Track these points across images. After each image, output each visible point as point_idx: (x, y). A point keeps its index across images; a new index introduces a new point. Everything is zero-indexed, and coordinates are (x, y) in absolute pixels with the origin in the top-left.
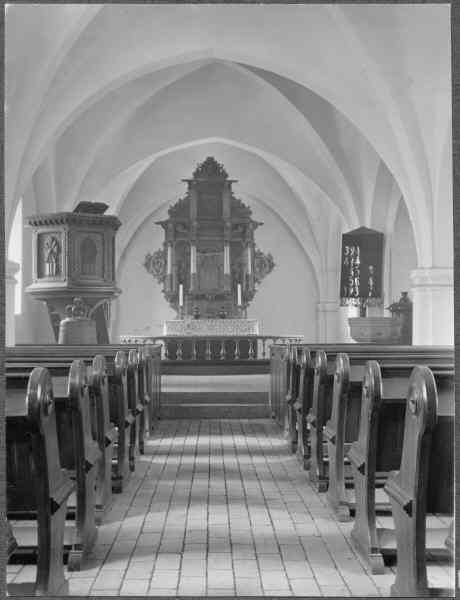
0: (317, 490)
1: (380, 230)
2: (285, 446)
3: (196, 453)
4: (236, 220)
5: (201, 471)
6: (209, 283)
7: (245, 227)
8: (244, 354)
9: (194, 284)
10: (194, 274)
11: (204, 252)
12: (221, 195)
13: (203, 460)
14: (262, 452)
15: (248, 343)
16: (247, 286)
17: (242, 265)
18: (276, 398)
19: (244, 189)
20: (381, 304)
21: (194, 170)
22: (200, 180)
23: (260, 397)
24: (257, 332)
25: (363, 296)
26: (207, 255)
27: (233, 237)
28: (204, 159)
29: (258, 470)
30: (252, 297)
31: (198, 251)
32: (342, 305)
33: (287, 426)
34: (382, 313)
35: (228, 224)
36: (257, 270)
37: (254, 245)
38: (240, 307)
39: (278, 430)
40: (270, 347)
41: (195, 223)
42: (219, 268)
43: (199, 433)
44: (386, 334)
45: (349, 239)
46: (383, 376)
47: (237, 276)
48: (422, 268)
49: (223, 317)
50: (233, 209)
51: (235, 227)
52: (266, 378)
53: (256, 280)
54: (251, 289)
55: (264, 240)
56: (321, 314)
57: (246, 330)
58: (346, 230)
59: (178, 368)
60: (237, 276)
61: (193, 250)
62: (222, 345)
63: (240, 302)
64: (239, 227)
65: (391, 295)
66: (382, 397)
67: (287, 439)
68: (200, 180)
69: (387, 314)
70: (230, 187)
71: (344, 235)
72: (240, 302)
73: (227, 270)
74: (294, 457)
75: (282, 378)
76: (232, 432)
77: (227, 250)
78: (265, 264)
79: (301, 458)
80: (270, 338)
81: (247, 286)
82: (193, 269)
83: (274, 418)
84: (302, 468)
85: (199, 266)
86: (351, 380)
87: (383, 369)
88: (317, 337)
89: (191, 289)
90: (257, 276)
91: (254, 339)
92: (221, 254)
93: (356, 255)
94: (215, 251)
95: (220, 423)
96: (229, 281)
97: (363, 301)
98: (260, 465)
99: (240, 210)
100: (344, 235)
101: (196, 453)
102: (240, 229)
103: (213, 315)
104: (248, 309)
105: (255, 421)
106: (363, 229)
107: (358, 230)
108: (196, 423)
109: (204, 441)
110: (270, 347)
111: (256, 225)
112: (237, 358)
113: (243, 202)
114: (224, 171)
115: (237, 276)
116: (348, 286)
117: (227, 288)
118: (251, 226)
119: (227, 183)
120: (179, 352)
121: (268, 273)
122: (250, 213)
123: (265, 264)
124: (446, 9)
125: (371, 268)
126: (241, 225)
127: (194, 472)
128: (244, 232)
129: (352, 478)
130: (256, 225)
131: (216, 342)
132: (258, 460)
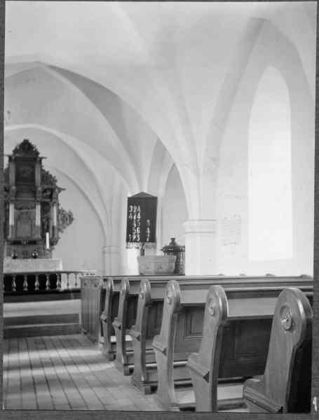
0: (143, 393)
1: (155, 195)
2: (100, 355)
3: (31, 366)
4: (46, 187)
5: (40, 383)
6: (24, 232)
7: (52, 191)
8: (53, 285)
9: (12, 232)
10: (12, 226)
11: (20, 209)
12: (33, 167)
13: (38, 373)
14: (86, 362)
15: (54, 277)
16: (53, 234)
17: (48, 219)
18: (87, 317)
19: (51, 163)
20: (155, 247)
21: (13, 148)
22: (17, 155)
23: (74, 318)
24: (60, 268)
25: (143, 240)
26: (22, 211)
27: (44, 198)
28: (22, 141)
29: (87, 378)
30: (57, 242)
31: (16, 208)
32: (127, 248)
33: (102, 339)
34: (155, 252)
35: (40, 189)
36: (61, 223)
37: (58, 205)
38: (48, 250)
39: (93, 342)
40: (80, 278)
41: (14, 188)
42: (32, 222)
43: (28, 349)
44: (165, 268)
45: (132, 201)
46: (228, 299)
47: (46, 227)
48: (193, 220)
49: (35, 257)
50: (43, 179)
51: (45, 191)
52: (78, 302)
53: (59, 230)
54: (56, 236)
55: (65, 201)
56: (107, 255)
57: (53, 267)
58: (130, 196)
59: (24, 297)
60: (45, 227)
61: (12, 207)
62: (48, 278)
63: (48, 246)
64: (48, 192)
65: (163, 239)
66: (228, 315)
67: (101, 350)
68: (17, 155)
69: (160, 253)
70: (40, 161)
71: (128, 198)
72: (48, 246)
73: (38, 222)
74: (112, 365)
75: (95, 302)
76: (55, 346)
77: (38, 208)
78: (67, 218)
79: (122, 366)
80: (73, 272)
81: (53, 234)
82: (11, 222)
83: (85, 333)
84: (122, 374)
85: (17, 219)
86: (182, 302)
87: (228, 293)
88: (104, 272)
89: (10, 237)
90: (60, 227)
91: (60, 273)
92: (33, 210)
93: (137, 213)
94: (28, 209)
95: (42, 339)
96: (40, 231)
97: (143, 245)
98: (88, 374)
99: (47, 178)
100: (128, 198)
101: (31, 366)
102: (49, 193)
103: (26, 256)
104: (53, 251)
105: (68, 337)
106: (143, 193)
107: (137, 195)
108: (31, 340)
109: (35, 356)
110: (80, 278)
111: (60, 190)
112: (47, 288)
113: (50, 173)
114: (36, 150)
115: (45, 227)
116: (132, 234)
117: (38, 236)
118: (56, 190)
119: (39, 159)
120: (37, 283)
121: (68, 225)
122: (56, 181)
123: (67, 218)
124: (316, 2)
125: (148, 221)
126: (48, 189)
127: (34, 384)
128: (52, 194)
129: (190, 379)
130: (60, 190)
131: (31, 277)
132: (83, 369)
